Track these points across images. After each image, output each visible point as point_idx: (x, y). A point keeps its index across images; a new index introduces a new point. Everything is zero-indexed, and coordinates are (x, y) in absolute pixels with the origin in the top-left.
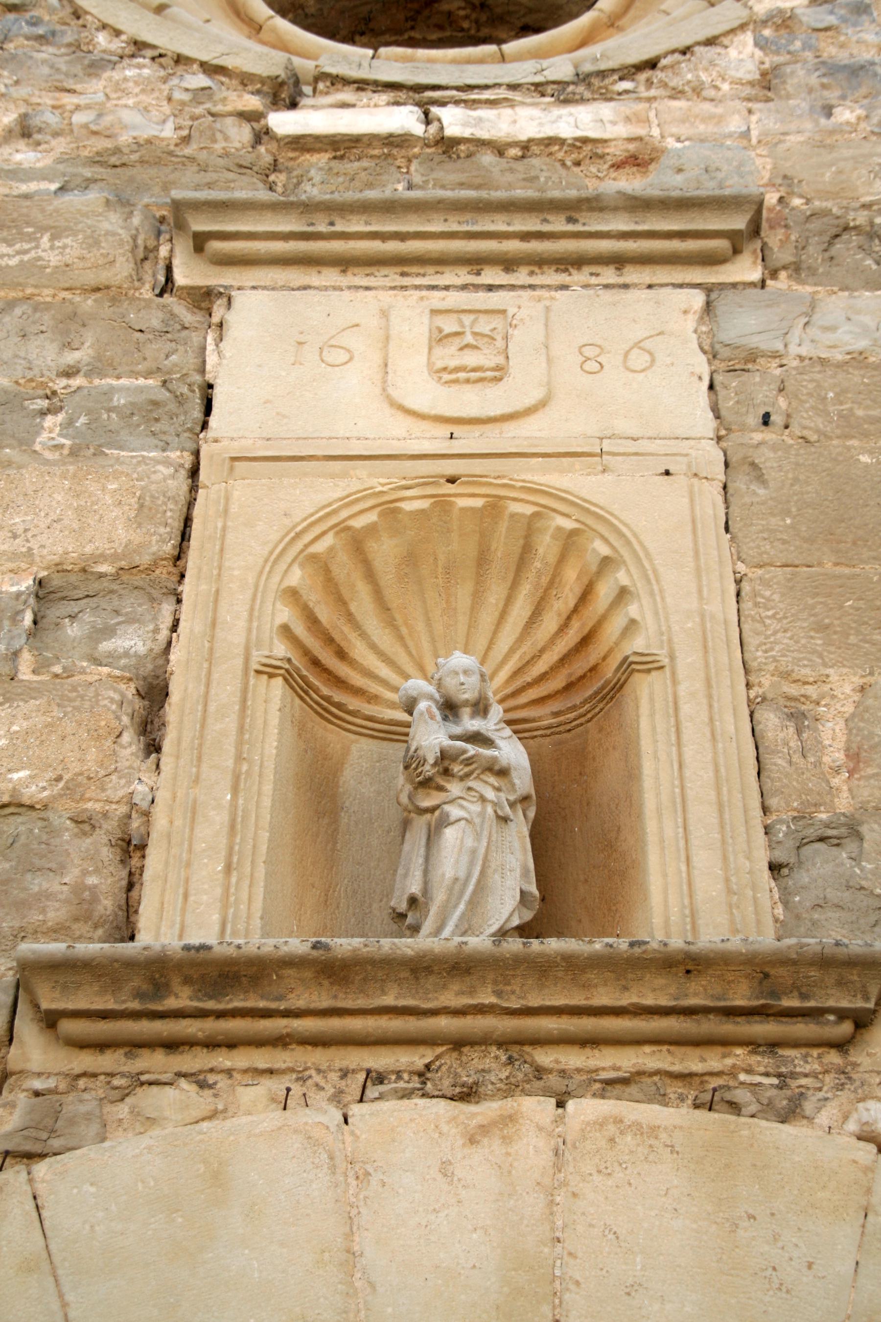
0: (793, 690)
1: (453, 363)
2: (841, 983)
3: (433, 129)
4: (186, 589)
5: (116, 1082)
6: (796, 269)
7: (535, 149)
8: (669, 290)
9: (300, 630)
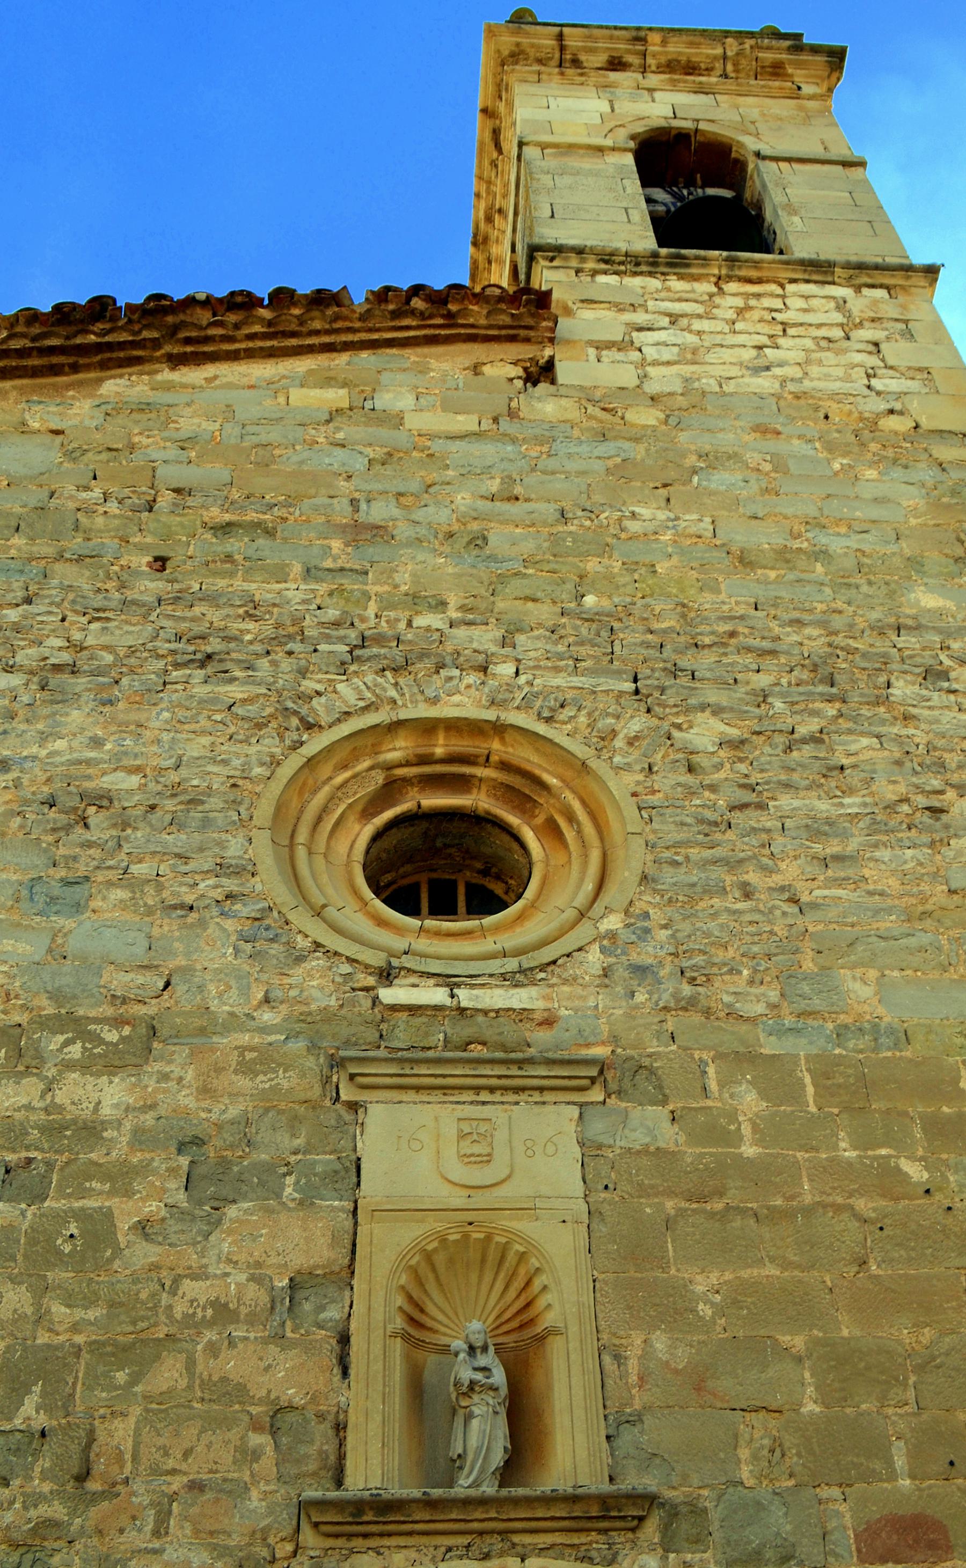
0: (617, 1342)
1: (469, 1152)
2: (634, 1504)
3: (455, 1000)
4: (355, 1282)
5: (344, 1552)
6: (620, 1093)
7: (502, 1013)
8: (563, 1106)
9: (408, 1308)
